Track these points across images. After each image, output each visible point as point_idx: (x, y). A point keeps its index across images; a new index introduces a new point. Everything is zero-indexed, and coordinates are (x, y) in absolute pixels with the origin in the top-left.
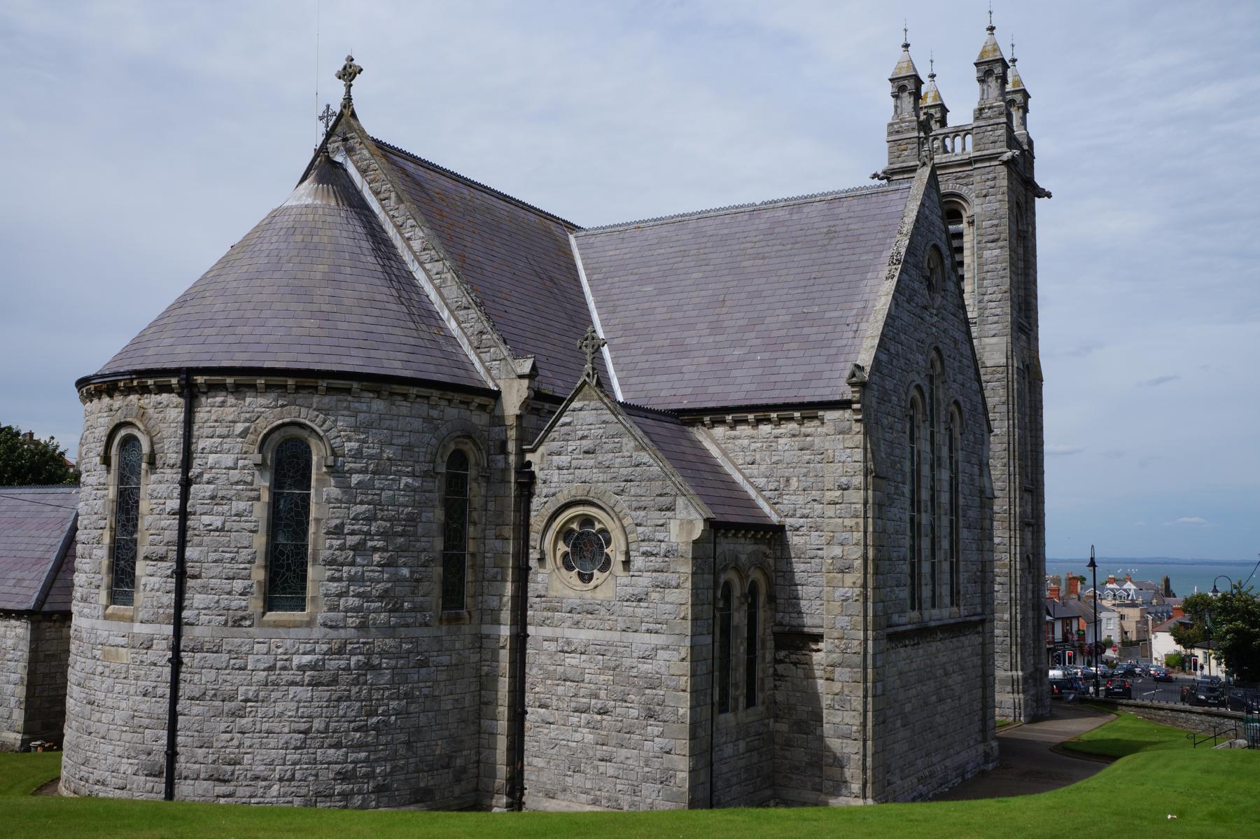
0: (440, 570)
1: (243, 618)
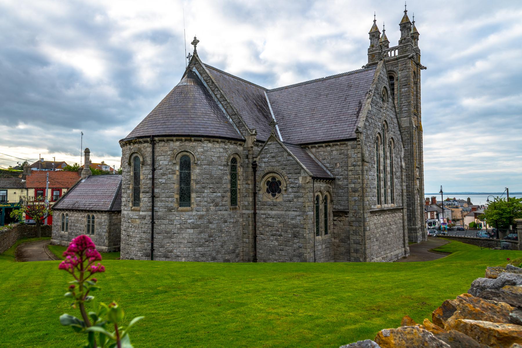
0: (230, 194)
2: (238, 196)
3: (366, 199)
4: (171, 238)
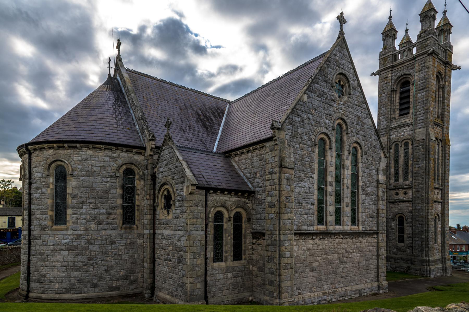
0: (121, 211)
1: (46, 228)
2: (137, 213)
3: (284, 217)
4: (44, 260)
